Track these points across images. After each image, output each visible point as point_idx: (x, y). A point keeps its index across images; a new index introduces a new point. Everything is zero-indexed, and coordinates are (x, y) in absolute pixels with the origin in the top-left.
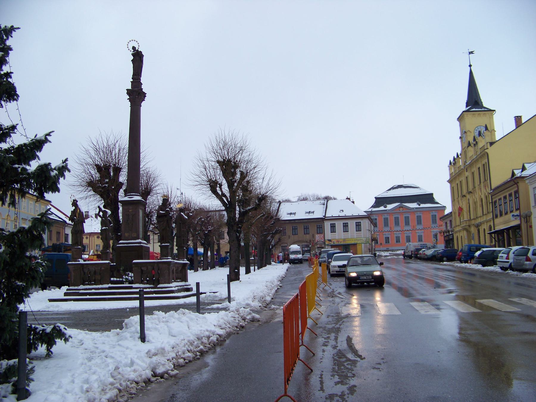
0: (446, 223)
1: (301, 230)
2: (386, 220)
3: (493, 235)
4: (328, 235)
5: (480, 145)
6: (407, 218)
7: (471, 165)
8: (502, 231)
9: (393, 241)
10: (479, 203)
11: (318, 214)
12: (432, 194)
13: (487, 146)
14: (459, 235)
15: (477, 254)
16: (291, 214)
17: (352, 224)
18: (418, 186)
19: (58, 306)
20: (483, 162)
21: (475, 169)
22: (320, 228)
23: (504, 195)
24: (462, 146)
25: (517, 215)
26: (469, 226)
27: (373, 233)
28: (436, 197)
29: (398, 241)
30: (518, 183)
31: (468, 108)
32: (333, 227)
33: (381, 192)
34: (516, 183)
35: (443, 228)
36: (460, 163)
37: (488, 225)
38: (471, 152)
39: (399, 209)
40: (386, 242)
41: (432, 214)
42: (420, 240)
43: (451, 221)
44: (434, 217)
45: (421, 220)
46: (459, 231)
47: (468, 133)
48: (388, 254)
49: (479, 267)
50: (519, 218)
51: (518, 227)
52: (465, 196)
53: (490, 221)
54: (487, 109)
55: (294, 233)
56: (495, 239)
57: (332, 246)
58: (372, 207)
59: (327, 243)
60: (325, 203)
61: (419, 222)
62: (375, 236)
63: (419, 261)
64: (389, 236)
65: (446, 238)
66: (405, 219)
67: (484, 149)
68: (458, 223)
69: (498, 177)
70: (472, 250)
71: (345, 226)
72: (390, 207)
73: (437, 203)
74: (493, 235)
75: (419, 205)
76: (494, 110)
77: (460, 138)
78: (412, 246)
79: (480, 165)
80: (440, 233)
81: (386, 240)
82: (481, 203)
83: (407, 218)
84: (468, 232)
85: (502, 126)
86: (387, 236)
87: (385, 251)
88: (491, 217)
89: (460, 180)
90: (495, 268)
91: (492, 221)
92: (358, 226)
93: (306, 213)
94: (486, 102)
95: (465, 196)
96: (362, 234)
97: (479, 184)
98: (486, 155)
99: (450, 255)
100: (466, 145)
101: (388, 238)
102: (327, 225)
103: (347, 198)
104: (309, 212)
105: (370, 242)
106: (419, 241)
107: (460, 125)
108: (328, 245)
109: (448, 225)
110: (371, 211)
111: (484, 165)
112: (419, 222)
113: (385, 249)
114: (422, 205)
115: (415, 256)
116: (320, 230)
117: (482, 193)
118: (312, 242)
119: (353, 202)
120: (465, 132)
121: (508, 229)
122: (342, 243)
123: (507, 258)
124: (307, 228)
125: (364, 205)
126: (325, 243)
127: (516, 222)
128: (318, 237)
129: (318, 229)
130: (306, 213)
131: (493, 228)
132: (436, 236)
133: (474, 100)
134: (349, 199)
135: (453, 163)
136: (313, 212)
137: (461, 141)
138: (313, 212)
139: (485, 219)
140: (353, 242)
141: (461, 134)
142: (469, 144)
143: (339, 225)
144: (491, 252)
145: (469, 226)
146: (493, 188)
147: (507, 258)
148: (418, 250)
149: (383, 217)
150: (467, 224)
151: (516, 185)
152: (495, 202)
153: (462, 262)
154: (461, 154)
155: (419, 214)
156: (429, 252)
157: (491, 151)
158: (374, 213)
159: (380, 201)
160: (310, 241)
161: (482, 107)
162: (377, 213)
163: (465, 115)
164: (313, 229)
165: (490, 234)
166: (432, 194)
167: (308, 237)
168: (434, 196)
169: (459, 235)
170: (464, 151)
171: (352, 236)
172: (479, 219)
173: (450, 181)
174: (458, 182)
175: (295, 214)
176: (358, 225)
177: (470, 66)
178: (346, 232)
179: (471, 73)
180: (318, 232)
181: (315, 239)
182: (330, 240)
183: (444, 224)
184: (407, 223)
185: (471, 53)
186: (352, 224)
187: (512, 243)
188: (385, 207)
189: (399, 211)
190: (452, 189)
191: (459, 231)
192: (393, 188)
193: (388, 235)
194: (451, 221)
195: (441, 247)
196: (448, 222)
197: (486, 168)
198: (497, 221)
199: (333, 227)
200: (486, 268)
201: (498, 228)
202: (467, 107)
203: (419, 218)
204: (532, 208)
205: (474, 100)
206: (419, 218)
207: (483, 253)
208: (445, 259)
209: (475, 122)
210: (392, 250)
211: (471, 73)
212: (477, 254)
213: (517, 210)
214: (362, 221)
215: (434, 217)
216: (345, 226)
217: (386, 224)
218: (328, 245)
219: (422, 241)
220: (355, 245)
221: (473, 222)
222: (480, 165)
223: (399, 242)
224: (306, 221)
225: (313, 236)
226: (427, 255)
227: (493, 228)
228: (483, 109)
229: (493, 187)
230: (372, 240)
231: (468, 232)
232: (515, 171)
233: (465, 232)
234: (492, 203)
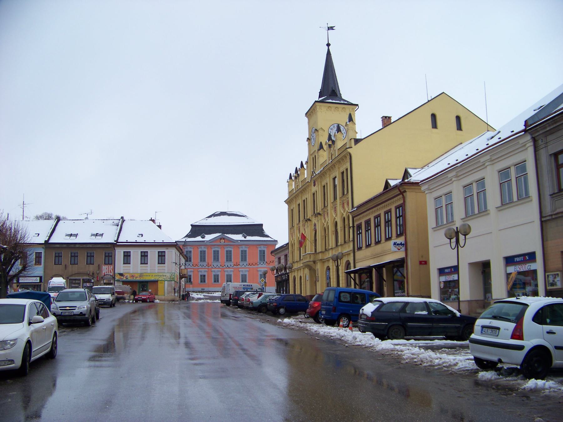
0: (279, 259)
1: (82, 258)
2: (203, 253)
3: (352, 275)
4: (120, 267)
5: (339, 144)
6: (229, 254)
7: (322, 174)
8: (368, 270)
9: (210, 279)
10: (331, 229)
11: (109, 238)
12: (262, 225)
13: (350, 144)
14: (297, 275)
15: (369, 309)
16: (71, 235)
17: (153, 254)
18: (245, 214)
19: (333, 278)
20: (343, 169)
21: (328, 180)
22: (109, 256)
23: (367, 218)
24: (309, 151)
25: (401, 244)
26: (314, 262)
27: (183, 267)
28: (267, 230)
29: (216, 280)
30: (405, 191)
31: (321, 99)
32: (127, 256)
33: (201, 220)
34: (402, 193)
35: (276, 265)
36: (306, 174)
37: (325, 267)
38: (324, 157)
39: (219, 241)
40: (201, 282)
41: (259, 249)
42: (244, 280)
43: (286, 256)
44: (262, 253)
45: (246, 256)
46: (298, 269)
47: (320, 132)
48: (202, 297)
49: (367, 339)
50: (403, 249)
51: (400, 264)
52: (309, 220)
53: (349, 254)
54: (347, 102)
55: (73, 262)
56: (355, 280)
57: (125, 283)
58: (186, 236)
59: (117, 278)
60: (120, 224)
61: (244, 258)
62: (185, 272)
63: (240, 314)
64: (206, 274)
65: (279, 279)
66: (227, 253)
67: (345, 148)
68: (297, 258)
69: (366, 188)
70: (342, 299)
71: (144, 256)
72: (208, 237)
73: (268, 236)
74: (352, 275)
75: (245, 237)
76: (357, 105)
77: (308, 139)
78: (233, 287)
79: (337, 173)
80: (272, 270)
81: (201, 279)
82: (334, 229)
83: (229, 254)
84: (313, 271)
85: (366, 124)
86: (203, 274)
87: (199, 292)
88: (351, 247)
89: (304, 198)
90: (463, 360)
91: (352, 255)
92: (162, 257)
93: (92, 235)
94: (346, 93)
95: (309, 220)
96: (166, 268)
97: (332, 200)
98: (348, 157)
99: (293, 306)
100: (317, 147)
101: (204, 276)
102: (119, 254)
103: (151, 220)
104: (97, 235)
105: (177, 279)
106: (242, 281)
107: (309, 123)
108: (118, 281)
109: (283, 261)
110: (185, 242)
111: (343, 173)
112: (244, 258)
113: (200, 289)
114: (249, 238)
115: (234, 302)
116: (110, 259)
117: (338, 214)
118: (96, 276)
119: (160, 226)
120: (316, 130)
121: (379, 268)
122: (138, 279)
123: (518, 334)
124: (91, 256)
125: (177, 232)
126: (114, 278)
127: (400, 255)
128: (105, 269)
129: (107, 258)
130: (92, 235)
131: (352, 265)
132: (265, 274)
133: (330, 90)
134: (153, 221)
135: (296, 176)
136: (102, 235)
137: (309, 144)
138: (102, 235)
139: (330, 255)
140: (152, 278)
141: (310, 134)
142: (321, 147)
143: (136, 254)
144: (400, 306)
145: (314, 262)
146: (356, 204)
147: (518, 334)
148: (238, 293)
149: (200, 250)
150: (312, 259)
151: (401, 196)
152: (359, 227)
153: (317, 321)
154: (307, 162)
155: (244, 248)
156: (255, 299)
157: (355, 151)
158: (188, 244)
159: (197, 230)
160: (93, 274)
161: (341, 99)
162: (191, 244)
163: (318, 107)
164: (99, 257)
165: (348, 273)
166: (262, 225)
167: (91, 268)
168: (264, 227)
169: (297, 275)
170: (313, 158)
171: (152, 270)
172: (330, 251)
173: (288, 202)
174: (300, 201)
175: (76, 235)
176: (162, 256)
177: (328, 45)
178: (144, 264)
179: (329, 54)
180: (107, 262)
181: (102, 271)
182: (121, 275)
183: (277, 260)
184: (229, 259)
185: (331, 28)
186: (153, 254)
187: (385, 289)
188: (203, 237)
189: (219, 243)
190: (291, 212)
191: (298, 269)
192: (214, 215)
193: (203, 271)
194: (286, 256)
195: (271, 291)
196: (283, 258)
197: (347, 178)
198: (359, 254)
199: (127, 256)
200: (387, 345)
201: (360, 265)
202: (320, 97)
203: (244, 253)
204: (430, 231)
205: (330, 90)
206: (244, 253)
207: (383, 309)
208: (282, 310)
209: (329, 117)
210: (208, 292)
211: (329, 54)
212: (369, 309)
213: (398, 236)
214: (166, 251)
215: (262, 253)
216: (144, 256)
217: (203, 259)
218: (118, 281)
219: (245, 281)
220: (155, 282)
221: (320, 256)
222: (337, 173)
223: (218, 281)
224: (91, 246)
225: (99, 267)
226: (252, 303)
227: (352, 265)
228: (342, 102)
229: (357, 203)
230: (181, 277)
231: (313, 271)
232: (389, 181)
233: (307, 271)
234: (353, 227)
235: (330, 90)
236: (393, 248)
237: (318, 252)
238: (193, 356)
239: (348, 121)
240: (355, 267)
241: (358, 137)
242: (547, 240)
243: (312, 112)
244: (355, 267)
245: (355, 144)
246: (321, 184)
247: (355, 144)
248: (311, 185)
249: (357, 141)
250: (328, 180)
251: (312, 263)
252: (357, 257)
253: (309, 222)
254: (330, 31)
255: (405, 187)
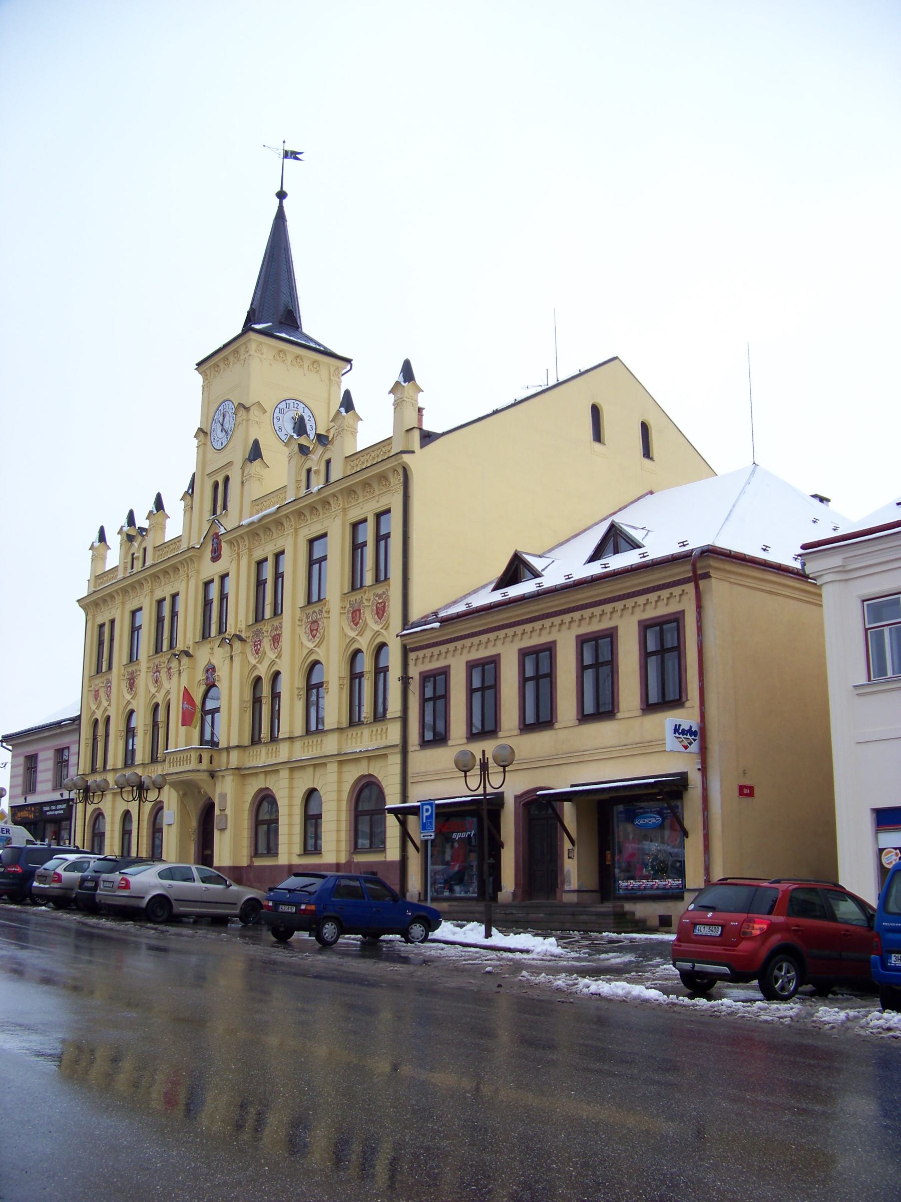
25: (690, 732)
30: (707, 576)
34: (697, 578)
51: (671, 790)
76: (349, 361)
91: (395, 760)
133: (275, 307)
137: (397, 405)
145: (212, 774)
150: (205, 765)
157: (421, 462)
163: (253, 346)
173: (90, 604)
177: (281, 195)
179: (280, 218)
205: (275, 307)
211: (280, 218)
235: (282, 308)
236: (671, 742)
237: (108, 768)
238: (162, 944)
239: (401, 380)
240: (404, 799)
241: (429, 425)
242: (86, 938)
243: (226, 359)
244: (404, 799)
245: (422, 446)
246: (251, 555)
247: (422, 446)
248: (200, 558)
249: (428, 438)
250: (293, 547)
251: (205, 776)
252: (411, 770)
253: (185, 660)
254: (289, 162)
255: (712, 562)
